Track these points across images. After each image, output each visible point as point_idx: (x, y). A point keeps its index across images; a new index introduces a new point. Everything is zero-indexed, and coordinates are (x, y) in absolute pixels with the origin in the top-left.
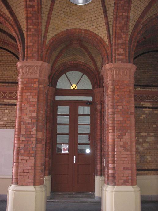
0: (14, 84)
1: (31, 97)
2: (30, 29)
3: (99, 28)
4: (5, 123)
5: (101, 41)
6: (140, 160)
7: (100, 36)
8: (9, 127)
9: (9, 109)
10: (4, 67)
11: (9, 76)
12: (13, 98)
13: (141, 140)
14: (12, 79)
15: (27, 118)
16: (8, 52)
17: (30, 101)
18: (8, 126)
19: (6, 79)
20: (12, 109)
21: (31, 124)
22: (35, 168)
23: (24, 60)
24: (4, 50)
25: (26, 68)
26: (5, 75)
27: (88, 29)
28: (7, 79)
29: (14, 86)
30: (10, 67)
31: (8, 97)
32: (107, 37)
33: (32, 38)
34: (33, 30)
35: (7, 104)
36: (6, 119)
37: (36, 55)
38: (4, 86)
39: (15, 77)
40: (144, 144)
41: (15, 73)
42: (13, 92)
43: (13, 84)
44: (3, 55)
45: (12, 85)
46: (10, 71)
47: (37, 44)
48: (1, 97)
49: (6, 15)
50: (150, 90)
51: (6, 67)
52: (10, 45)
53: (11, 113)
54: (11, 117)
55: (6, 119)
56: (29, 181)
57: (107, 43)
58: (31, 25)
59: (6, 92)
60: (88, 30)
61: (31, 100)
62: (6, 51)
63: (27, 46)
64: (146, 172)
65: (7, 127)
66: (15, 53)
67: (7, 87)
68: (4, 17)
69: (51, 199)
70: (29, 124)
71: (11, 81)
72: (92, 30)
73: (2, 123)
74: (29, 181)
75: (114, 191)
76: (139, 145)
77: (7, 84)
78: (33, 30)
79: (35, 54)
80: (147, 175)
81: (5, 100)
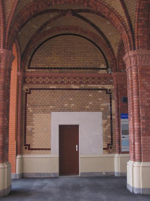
1: (147, 83)
2: (141, 20)
4: (90, 107)
8: (95, 111)
9: (93, 93)
10: (84, 54)
14: (92, 65)
15: (146, 102)
16: (86, 40)
17: (146, 87)
18: (93, 109)
19: (88, 65)
22: (120, 150)
23: (135, 49)
24: (82, 38)
25: (139, 56)
26: (86, 61)
28: (89, 66)
29: (96, 72)
30: (90, 54)
31: (90, 82)
33: (142, 29)
34: (143, 21)
35: (90, 89)
36: (91, 103)
37: (146, 44)
38: (86, 72)
39: (95, 63)
41: (95, 60)
42: (101, 78)
43: (94, 70)
44: (82, 43)
45: (93, 71)
46: (89, 58)
47: (147, 34)
49: (110, 6)
51: (86, 54)
52: (88, 33)
53: (95, 97)
54: (95, 101)
55: (91, 103)
58: (142, 17)
59: (95, 78)
62: (84, 39)
63: (138, 36)
66: (92, 40)
67: (89, 73)
68: (108, 8)
70: (147, 107)
71: (92, 67)
73: (88, 107)
75: (141, 166)
77: (88, 70)
78: (143, 21)
79: (146, 44)
81: (88, 85)
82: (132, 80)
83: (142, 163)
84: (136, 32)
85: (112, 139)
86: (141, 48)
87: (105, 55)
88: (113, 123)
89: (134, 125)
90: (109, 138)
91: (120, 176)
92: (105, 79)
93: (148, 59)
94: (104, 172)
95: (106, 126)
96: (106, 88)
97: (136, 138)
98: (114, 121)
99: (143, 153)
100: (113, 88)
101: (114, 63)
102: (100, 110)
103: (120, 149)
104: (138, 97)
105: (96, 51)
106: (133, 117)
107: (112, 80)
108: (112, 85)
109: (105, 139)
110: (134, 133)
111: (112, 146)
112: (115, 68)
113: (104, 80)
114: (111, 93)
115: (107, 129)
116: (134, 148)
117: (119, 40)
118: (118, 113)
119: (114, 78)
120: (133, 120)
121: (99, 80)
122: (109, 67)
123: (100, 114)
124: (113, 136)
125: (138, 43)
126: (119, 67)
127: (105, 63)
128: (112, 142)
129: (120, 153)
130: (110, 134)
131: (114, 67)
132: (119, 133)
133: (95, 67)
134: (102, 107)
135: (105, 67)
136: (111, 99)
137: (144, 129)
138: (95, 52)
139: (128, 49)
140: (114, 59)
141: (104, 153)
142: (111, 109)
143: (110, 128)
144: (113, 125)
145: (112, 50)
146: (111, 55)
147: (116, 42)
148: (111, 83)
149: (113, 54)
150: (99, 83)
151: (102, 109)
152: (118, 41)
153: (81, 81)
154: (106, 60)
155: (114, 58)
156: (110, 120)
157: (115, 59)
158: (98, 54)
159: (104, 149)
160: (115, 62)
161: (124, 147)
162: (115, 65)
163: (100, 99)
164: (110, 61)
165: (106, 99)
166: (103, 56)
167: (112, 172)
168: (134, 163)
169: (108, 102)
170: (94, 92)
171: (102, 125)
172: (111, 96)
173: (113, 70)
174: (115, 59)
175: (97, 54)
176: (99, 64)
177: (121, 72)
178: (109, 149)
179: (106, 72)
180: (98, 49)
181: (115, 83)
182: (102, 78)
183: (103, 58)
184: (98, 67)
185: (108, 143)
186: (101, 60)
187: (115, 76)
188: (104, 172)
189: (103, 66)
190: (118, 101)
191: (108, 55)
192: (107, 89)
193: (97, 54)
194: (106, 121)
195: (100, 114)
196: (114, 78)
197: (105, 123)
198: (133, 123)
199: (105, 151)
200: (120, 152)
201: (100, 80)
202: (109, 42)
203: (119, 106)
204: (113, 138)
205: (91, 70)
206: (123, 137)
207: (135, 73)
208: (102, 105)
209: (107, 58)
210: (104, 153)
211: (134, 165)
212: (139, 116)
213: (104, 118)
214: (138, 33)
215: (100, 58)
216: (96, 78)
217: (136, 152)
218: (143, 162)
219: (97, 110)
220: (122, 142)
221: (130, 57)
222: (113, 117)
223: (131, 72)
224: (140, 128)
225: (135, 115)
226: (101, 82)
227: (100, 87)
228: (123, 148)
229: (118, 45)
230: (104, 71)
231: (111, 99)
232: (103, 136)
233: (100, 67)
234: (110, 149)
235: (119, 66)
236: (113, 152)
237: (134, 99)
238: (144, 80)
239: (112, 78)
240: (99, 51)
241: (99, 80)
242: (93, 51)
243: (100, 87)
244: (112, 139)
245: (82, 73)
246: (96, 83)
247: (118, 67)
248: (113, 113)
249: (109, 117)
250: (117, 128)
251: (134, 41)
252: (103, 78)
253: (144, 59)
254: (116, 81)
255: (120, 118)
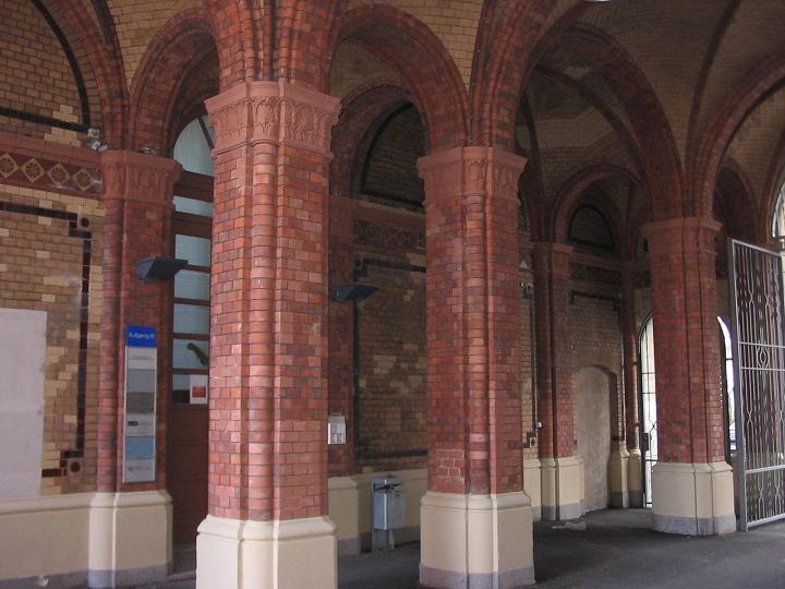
0: (33, 125)
3: (454, 30)
5: (451, 67)
6: (402, 424)
7: (451, 52)
8: (16, 303)
11: (12, 85)
12: (28, 181)
13: (404, 366)
14: (22, 99)
17: (301, 229)
20: (24, 226)
21: (308, 309)
25: (290, 108)
27: (425, 20)
29: (33, 133)
32: (469, 64)
33: (312, 7)
35: (20, 211)
40: (411, 378)
42: (56, 163)
43: (29, 124)
46: (13, 64)
48: (6, 175)
50: (391, 209)
56: (310, 502)
57: (467, 80)
59: (54, 163)
60: (424, 26)
61: (306, 226)
64: (414, 458)
65: (8, 301)
69: (175, 571)
71: (20, 108)
72: (434, 29)
74: (310, 502)
76: (400, 379)
80: (415, 468)
82: (249, 198)
83: (277, 523)
84: (288, 13)
85: (81, 429)
86: (299, 78)
87: (82, 69)
88: (89, 360)
89: (245, 376)
90: (70, 425)
91: (113, 585)
92: (73, 169)
93: (316, 128)
94: (45, 577)
95: (61, 373)
96: (70, 209)
97: (253, 426)
98: (96, 352)
99: (281, 487)
100: (102, 213)
101: (118, 110)
102: (40, 300)
103: (114, 472)
104: (273, 268)
105: (45, 40)
106: (246, 345)
107: (100, 182)
108: (95, 203)
109: (52, 429)
110: (245, 408)
111: (79, 460)
112: (119, 133)
113: (68, 177)
114: (88, 235)
115: (62, 385)
116: (244, 465)
117: (164, 22)
118: (116, 322)
119: (111, 176)
120: (245, 354)
121: (42, 173)
122: (93, 123)
123: (36, 320)
124: (88, 419)
125: (289, 58)
126: (135, 130)
127: (79, 104)
128: (80, 443)
129: (115, 490)
130: (76, 410)
131: (113, 130)
132: (116, 406)
133: (33, 111)
134: (49, 289)
135: (74, 120)
136: (87, 258)
137: (287, 393)
138: (40, 47)
139: (244, 71)
140: (121, 94)
141: (44, 492)
142: (85, 302)
143: (75, 385)
144: (90, 369)
145: (116, 54)
146: (105, 75)
147: (146, 25)
148: (92, 193)
149: (119, 69)
150: (43, 184)
151: (48, 298)
152: (155, 23)
153: (45, 176)
154: (83, 92)
155: (122, 91)
156: (77, 350)
157: (121, 96)
158: (54, 59)
159: (46, 473)
160: (123, 106)
161: (133, 463)
162: (119, 117)
163: (41, 254)
164: (97, 100)
165: (68, 257)
166: (71, 72)
167: (80, 573)
168: (242, 526)
169: (75, 272)
170: (17, 222)
171: (41, 370)
172: (87, 245)
173: (109, 140)
174: (121, 96)
175: (46, 57)
176: (53, 101)
177: (142, 152)
178: (65, 474)
179: (78, 144)
180: (52, 33)
181: (111, 193)
182: (59, 166)
183: (73, 79)
184: (44, 113)
185: (66, 446)
186: (64, 85)
187: (118, 166)
188: (45, 577)
189: (67, 113)
190: (118, 271)
191: (92, 71)
192: (73, 216)
193: (46, 57)
194: (62, 351)
195: (36, 320)
196: (111, 176)
197: (55, 360)
198: (245, 365)
199: (51, 480)
200: (113, 487)
201: (49, 173)
202: (111, 18)
203: (123, 294)
204: (87, 427)
205: (13, 120)
206: (132, 423)
207: (269, 171)
208: (47, 281)
209: (88, 85)
210: (44, 492)
211: (244, 537)
212: (271, 342)
213: (54, 338)
214: (293, 20)
215: (58, 76)
216: (33, 161)
217: (251, 481)
218: (498, 492)
219: (29, 301)
220: (123, 443)
221: (249, 105)
222: (93, 336)
223: (250, 162)
224: (271, 390)
225: (253, 338)
226: (52, 183)
227: (46, 200)
228: (130, 469)
229: (148, 41)
230: (70, 138)
231: (87, 258)
232: (45, 419)
233: (56, 115)
234: (71, 473)
235: (135, 125)
236: (87, 484)
237: (256, 273)
238: (297, 203)
239: (100, 172)
240: (58, 44)
241: (46, 169)
242: (34, 37)
243: (46, 200)
244: (81, 429)
245: (16, 132)
246: (33, 180)
247: (131, 132)
248: (91, 320)
249: (74, 335)
250: (104, 385)
251: (274, 46)
252: (37, 159)
253: (303, 123)
254: (116, 187)
255: (121, 343)
